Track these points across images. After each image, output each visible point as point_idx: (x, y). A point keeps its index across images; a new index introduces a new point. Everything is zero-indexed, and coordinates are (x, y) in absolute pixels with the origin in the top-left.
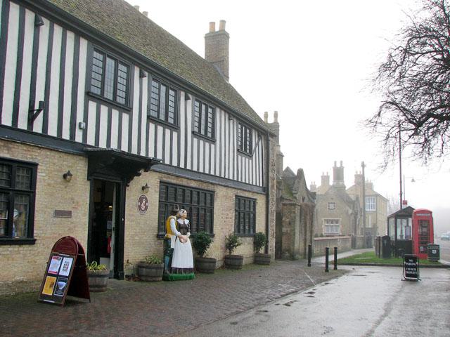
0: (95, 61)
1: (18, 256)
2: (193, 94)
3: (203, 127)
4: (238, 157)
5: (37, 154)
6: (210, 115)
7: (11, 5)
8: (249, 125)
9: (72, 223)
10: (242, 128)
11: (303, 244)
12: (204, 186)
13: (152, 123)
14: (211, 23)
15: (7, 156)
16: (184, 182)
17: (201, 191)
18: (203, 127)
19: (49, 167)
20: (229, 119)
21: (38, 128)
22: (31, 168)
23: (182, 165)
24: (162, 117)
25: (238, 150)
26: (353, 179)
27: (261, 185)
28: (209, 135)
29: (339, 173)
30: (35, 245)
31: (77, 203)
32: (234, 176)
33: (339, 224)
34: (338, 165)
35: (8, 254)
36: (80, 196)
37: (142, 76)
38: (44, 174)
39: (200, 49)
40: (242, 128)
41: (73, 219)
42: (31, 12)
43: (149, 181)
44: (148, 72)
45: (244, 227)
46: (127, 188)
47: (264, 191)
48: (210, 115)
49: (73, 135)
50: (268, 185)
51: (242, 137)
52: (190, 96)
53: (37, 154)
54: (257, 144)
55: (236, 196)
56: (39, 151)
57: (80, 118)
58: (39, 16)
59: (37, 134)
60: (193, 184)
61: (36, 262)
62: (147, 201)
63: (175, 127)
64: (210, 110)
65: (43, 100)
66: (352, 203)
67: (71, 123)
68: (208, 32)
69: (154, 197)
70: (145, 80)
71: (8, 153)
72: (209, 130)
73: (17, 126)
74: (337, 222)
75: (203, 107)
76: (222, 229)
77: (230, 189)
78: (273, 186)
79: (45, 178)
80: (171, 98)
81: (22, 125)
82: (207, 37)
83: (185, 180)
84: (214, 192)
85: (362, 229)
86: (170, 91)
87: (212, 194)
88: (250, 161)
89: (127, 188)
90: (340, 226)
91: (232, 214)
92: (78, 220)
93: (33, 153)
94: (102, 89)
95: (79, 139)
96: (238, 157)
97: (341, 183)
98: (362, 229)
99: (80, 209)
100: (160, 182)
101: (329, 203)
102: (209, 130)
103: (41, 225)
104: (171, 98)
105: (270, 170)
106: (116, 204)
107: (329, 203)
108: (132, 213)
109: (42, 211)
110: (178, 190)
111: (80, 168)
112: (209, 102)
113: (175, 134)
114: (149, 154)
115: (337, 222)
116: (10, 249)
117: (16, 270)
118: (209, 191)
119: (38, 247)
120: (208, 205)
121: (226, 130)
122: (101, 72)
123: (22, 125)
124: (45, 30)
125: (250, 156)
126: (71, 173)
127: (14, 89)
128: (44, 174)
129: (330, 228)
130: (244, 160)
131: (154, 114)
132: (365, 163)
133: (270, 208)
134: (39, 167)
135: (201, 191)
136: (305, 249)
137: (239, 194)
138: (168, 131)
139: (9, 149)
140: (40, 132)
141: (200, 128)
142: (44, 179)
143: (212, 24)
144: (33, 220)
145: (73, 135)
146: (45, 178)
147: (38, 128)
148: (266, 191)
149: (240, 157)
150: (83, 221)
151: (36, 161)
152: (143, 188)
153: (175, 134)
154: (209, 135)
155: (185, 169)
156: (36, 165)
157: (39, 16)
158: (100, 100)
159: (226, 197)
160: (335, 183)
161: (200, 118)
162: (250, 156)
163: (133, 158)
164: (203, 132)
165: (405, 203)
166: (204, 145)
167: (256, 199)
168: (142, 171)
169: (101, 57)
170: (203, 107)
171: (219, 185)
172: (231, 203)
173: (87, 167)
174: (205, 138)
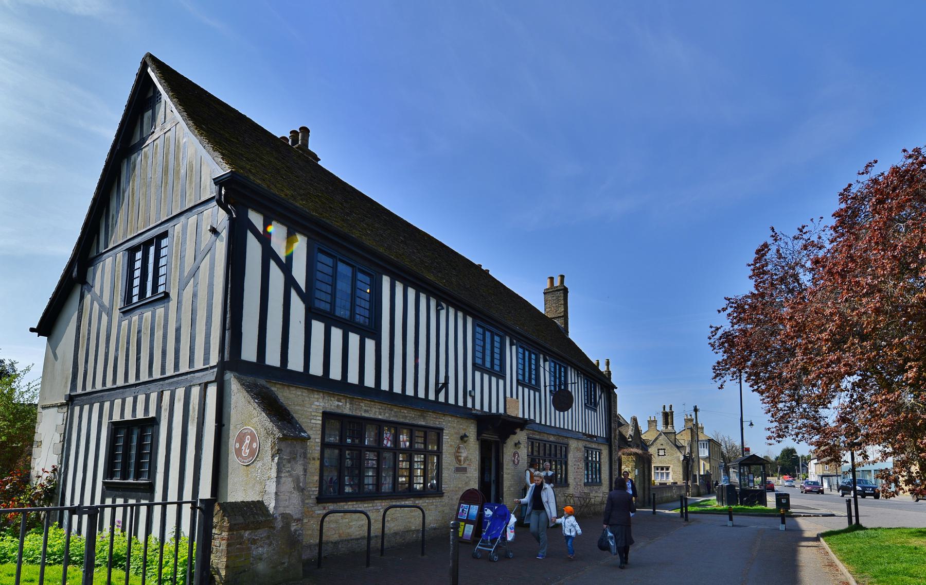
0: (320, 267)
1: (432, 507)
2: (550, 356)
4: (585, 411)
5: (442, 421)
6: (533, 362)
7: (421, 295)
8: (593, 379)
9: (467, 477)
10: (484, 335)
11: (642, 493)
12: (561, 440)
13: (494, 376)
15: (423, 423)
16: (545, 437)
17: (558, 445)
19: (451, 429)
20: (578, 377)
21: (442, 399)
22: (439, 432)
24: (488, 365)
25: (585, 404)
27: (604, 436)
30: (443, 498)
31: (470, 460)
34: (667, 410)
35: (426, 506)
36: (472, 453)
37: (511, 344)
38: (448, 437)
40: (484, 335)
42: (434, 299)
43: (521, 436)
44: (549, 357)
45: (592, 476)
46: (505, 445)
47: (607, 442)
48: (533, 362)
49: (465, 402)
50: (611, 436)
51: (524, 365)
53: (442, 421)
54: (600, 397)
56: (444, 418)
57: (469, 388)
60: (552, 439)
61: (443, 512)
62: (518, 456)
63: (501, 375)
64: (533, 356)
69: (524, 452)
70: (514, 348)
71: (423, 421)
73: (309, 372)
74: (668, 469)
75: (527, 353)
76: (575, 478)
78: (615, 436)
79: (449, 440)
80: (497, 345)
81: (432, 397)
83: (546, 435)
84: (568, 445)
86: (477, 328)
88: (595, 413)
89: (505, 445)
92: (471, 475)
93: (439, 420)
94: (333, 304)
96: (585, 411)
99: (472, 465)
100: (528, 438)
101: (658, 449)
103: (446, 481)
104: (497, 345)
105: (612, 421)
106: (496, 460)
107: (658, 449)
108: (508, 467)
109: (447, 468)
110: (534, 443)
111: (471, 431)
112: (562, 362)
116: (427, 501)
117: (431, 519)
118: (548, 442)
119: (445, 499)
120: (563, 457)
121: (576, 387)
122: (482, 344)
123: (432, 397)
124: (443, 313)
125: (595, 411)
126: (468, 434)
127: (425, 367)
128: (448, 437)
130: (590, 413)
131: (479, 361)
133: (613, 457)
134: (444, 431)
136: (644, 497)
137: (587, 446)
138: (494, 379)
139: (424, 418)
140: (443, 401)
141: (524, 375)
142: (447, 441)
145: (465, 402)
146: (449, 440)
149: (587, 410)
150: (475, 475)
151: (442, 426)
152: (516, 445)
153: (501, 382)
154: (533, 382)
156: (442, 429)
158: (524, 386)
159: (578, 449)
162: (595, 411)
163: (511, 419)
164: (488, 365)
165: (748, 450)
166: (588, 412)
168: (518, 431)
169: (329, 261)
170: (527, 353)
171: (572, 438)
173: (476, 428)
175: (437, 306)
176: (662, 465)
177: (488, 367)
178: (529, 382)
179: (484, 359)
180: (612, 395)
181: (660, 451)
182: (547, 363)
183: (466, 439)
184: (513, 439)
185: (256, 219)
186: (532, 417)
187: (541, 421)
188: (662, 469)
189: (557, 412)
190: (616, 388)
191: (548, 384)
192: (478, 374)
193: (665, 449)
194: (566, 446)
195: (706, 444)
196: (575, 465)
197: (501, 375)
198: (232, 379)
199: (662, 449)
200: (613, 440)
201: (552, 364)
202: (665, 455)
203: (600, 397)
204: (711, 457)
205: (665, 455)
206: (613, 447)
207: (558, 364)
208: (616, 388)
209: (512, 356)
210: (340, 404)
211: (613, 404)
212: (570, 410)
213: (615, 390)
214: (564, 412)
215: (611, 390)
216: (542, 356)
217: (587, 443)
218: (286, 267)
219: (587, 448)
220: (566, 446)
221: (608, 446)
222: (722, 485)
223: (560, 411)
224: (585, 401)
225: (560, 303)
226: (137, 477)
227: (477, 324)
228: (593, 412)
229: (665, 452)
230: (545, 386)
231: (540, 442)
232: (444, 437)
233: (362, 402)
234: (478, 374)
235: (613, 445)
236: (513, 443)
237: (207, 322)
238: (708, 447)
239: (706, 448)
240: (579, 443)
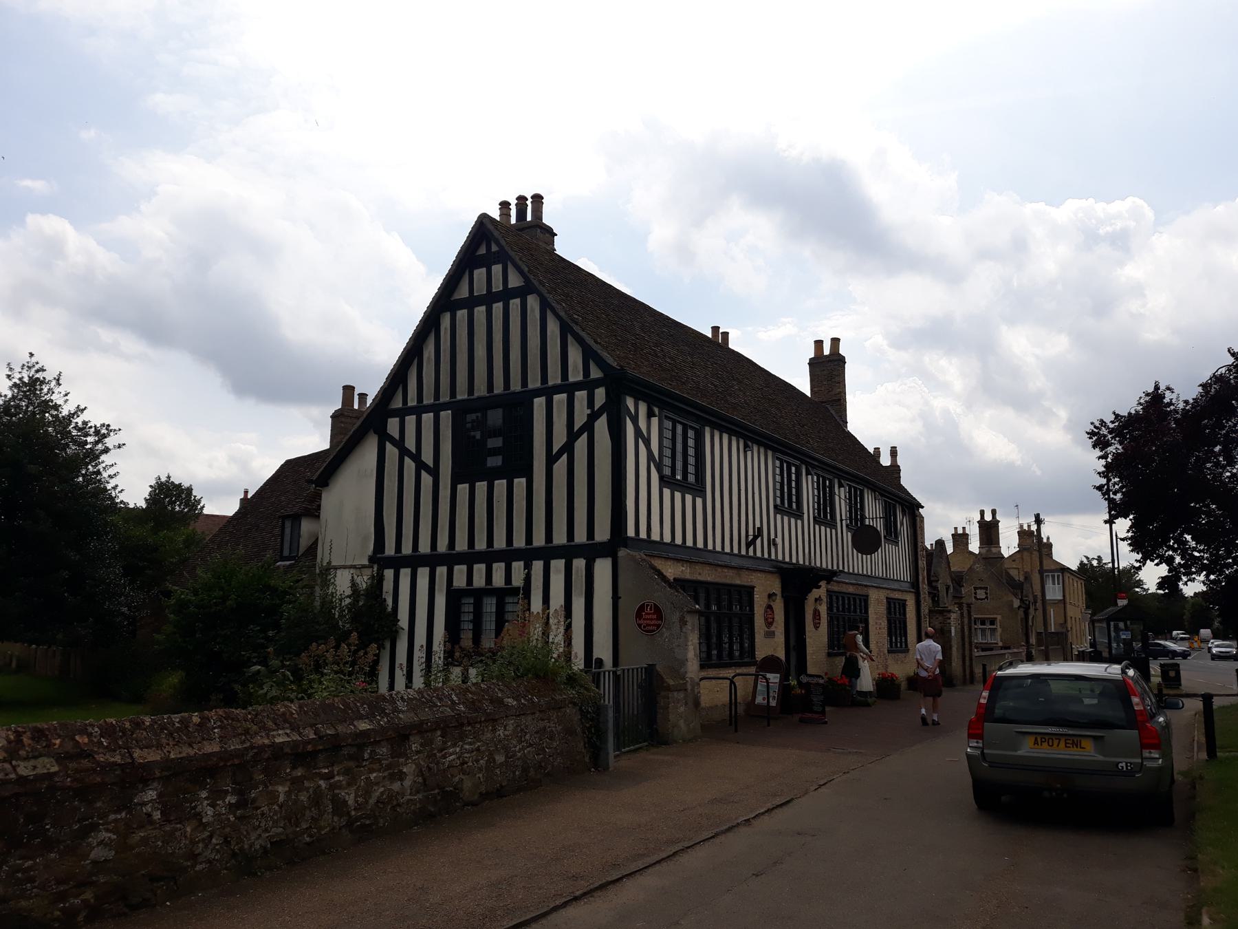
3: (679, 465)
14: (816, 342)
17: (857, 597)
18: (679, 465)
21: (751, 553)
23: (736, 551)
26: (1015, 540)
27: (909, 580)
28: (691, 478)
29: (989, 530)
32: (883, 573)
33: (998, 626)
34: (988, 517)
37: (807, 474)
39: (802, 383)
41: (776, 639)
48: (691, 443)
52: (656, 410)
55: (887, 598)
57: (772, 536)
58: (651, 405)
59: (689, 547)
60: (851, 589)
63: (798, 515)
64: (691, 433)
65: (759, 526)
66: (1016, 587)
67: (650, 519)
68: (813, 356)
72: (691, 469)
74: (993, 622)
77: (882, 590)
82: (812, 363)
85: (1039, 634)
87: (865, 599)
90: (999, 630)
91: (884, 623)
95: (773, 557)
97: (994, 550)
98: (1039, 634)
101: (976, 589)
102: (691, 469)
105: (919, 557)
112: (858, 484)
113: (699, 501)
114: (717, 547)
115: (993, 622)
118: (858, 595)
123: (743, 552)
125: (896, 544)
129: (988, 633)
132: (1042, 517)
135: (857, 597)
143: (819, 344)
144: (754, 642)
147: (751, 553)
148: (915, 584)
149: (779, 517)
152: (816, 600)
153: (799, 522)
154: (691, 478)
155: (695, 547)
156: (753, 588)
157: (651, 405)
160: (984, 551)
161: (1078, 577)
162: (896, 544)
167: (906, 600)
170: (679, 428)
172: (883, 609)
174: (683, 487)
175: (745, 448)
176: (983, 616)
177: (667, 474)
178: (825, 517)
179: (673, 468)
180: (918, 519)
181: (978, 591)
182: (842, 489)
183: (774, 598)
184: (815, 593)
185: (630, 403)
186: (841, 568)
187: (714, 547)
188: (983, 623)
189: (860, 555)
190: (922, 507)
191: (844, 518)
192: (667, 492)
193: (986, 588)
194: (865, 598)
195: (1058, 576)
196: (876, 623)
197: (798, 515)
198: (653, 562)
199: (981, 588)
200: (921, 586)
201: (668, 424)
202: (987, 598)
203: (902, 524)
204: (1068, 601)
205: (987, 598)
206: (922, 596)
207: (854, 487)
208: (922, 507)
209: (809, 488)
210: (684, 569)
211: (919, 532)
212: (876, 553)
213: (921, 510)
214: (871, 554)
215: (916, 512)
216: (836, 481)
217: (889, 591)
218: (647, 443)
219: (830, 591)
220: (865, 598)
221: (913, 594)
222: (1083, 651)
223: (867, 554)
224: (775, 500)
225: (833, 380)
226: (839, 649)
227: (666, 416)
228: (890, 546)
229: (986, 593)
230: (841, 520)
231: (838, 594)
232: (755, 596)
233: (752, 575)
234: (817, 527)
235: (922, 593)
236: (813, 599)
237: (1043, 613)
238: (1061, 581)
239: (1058, 584)
240: (880, 593)
